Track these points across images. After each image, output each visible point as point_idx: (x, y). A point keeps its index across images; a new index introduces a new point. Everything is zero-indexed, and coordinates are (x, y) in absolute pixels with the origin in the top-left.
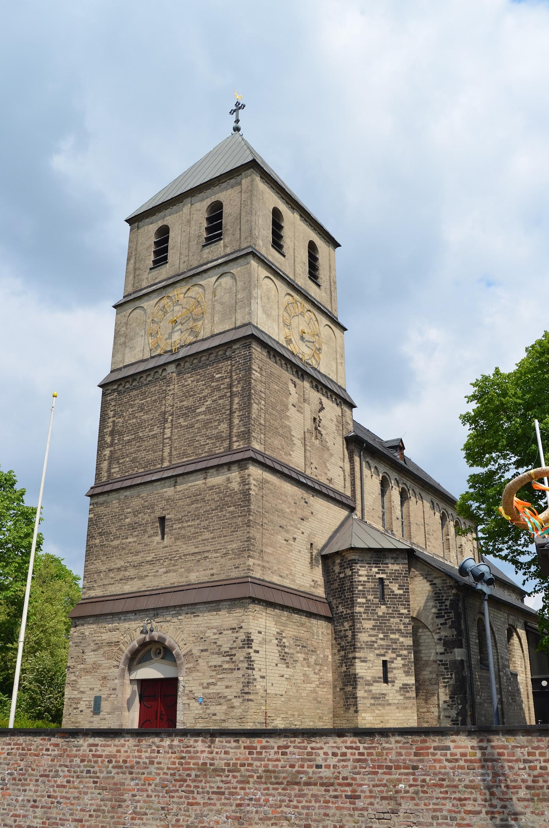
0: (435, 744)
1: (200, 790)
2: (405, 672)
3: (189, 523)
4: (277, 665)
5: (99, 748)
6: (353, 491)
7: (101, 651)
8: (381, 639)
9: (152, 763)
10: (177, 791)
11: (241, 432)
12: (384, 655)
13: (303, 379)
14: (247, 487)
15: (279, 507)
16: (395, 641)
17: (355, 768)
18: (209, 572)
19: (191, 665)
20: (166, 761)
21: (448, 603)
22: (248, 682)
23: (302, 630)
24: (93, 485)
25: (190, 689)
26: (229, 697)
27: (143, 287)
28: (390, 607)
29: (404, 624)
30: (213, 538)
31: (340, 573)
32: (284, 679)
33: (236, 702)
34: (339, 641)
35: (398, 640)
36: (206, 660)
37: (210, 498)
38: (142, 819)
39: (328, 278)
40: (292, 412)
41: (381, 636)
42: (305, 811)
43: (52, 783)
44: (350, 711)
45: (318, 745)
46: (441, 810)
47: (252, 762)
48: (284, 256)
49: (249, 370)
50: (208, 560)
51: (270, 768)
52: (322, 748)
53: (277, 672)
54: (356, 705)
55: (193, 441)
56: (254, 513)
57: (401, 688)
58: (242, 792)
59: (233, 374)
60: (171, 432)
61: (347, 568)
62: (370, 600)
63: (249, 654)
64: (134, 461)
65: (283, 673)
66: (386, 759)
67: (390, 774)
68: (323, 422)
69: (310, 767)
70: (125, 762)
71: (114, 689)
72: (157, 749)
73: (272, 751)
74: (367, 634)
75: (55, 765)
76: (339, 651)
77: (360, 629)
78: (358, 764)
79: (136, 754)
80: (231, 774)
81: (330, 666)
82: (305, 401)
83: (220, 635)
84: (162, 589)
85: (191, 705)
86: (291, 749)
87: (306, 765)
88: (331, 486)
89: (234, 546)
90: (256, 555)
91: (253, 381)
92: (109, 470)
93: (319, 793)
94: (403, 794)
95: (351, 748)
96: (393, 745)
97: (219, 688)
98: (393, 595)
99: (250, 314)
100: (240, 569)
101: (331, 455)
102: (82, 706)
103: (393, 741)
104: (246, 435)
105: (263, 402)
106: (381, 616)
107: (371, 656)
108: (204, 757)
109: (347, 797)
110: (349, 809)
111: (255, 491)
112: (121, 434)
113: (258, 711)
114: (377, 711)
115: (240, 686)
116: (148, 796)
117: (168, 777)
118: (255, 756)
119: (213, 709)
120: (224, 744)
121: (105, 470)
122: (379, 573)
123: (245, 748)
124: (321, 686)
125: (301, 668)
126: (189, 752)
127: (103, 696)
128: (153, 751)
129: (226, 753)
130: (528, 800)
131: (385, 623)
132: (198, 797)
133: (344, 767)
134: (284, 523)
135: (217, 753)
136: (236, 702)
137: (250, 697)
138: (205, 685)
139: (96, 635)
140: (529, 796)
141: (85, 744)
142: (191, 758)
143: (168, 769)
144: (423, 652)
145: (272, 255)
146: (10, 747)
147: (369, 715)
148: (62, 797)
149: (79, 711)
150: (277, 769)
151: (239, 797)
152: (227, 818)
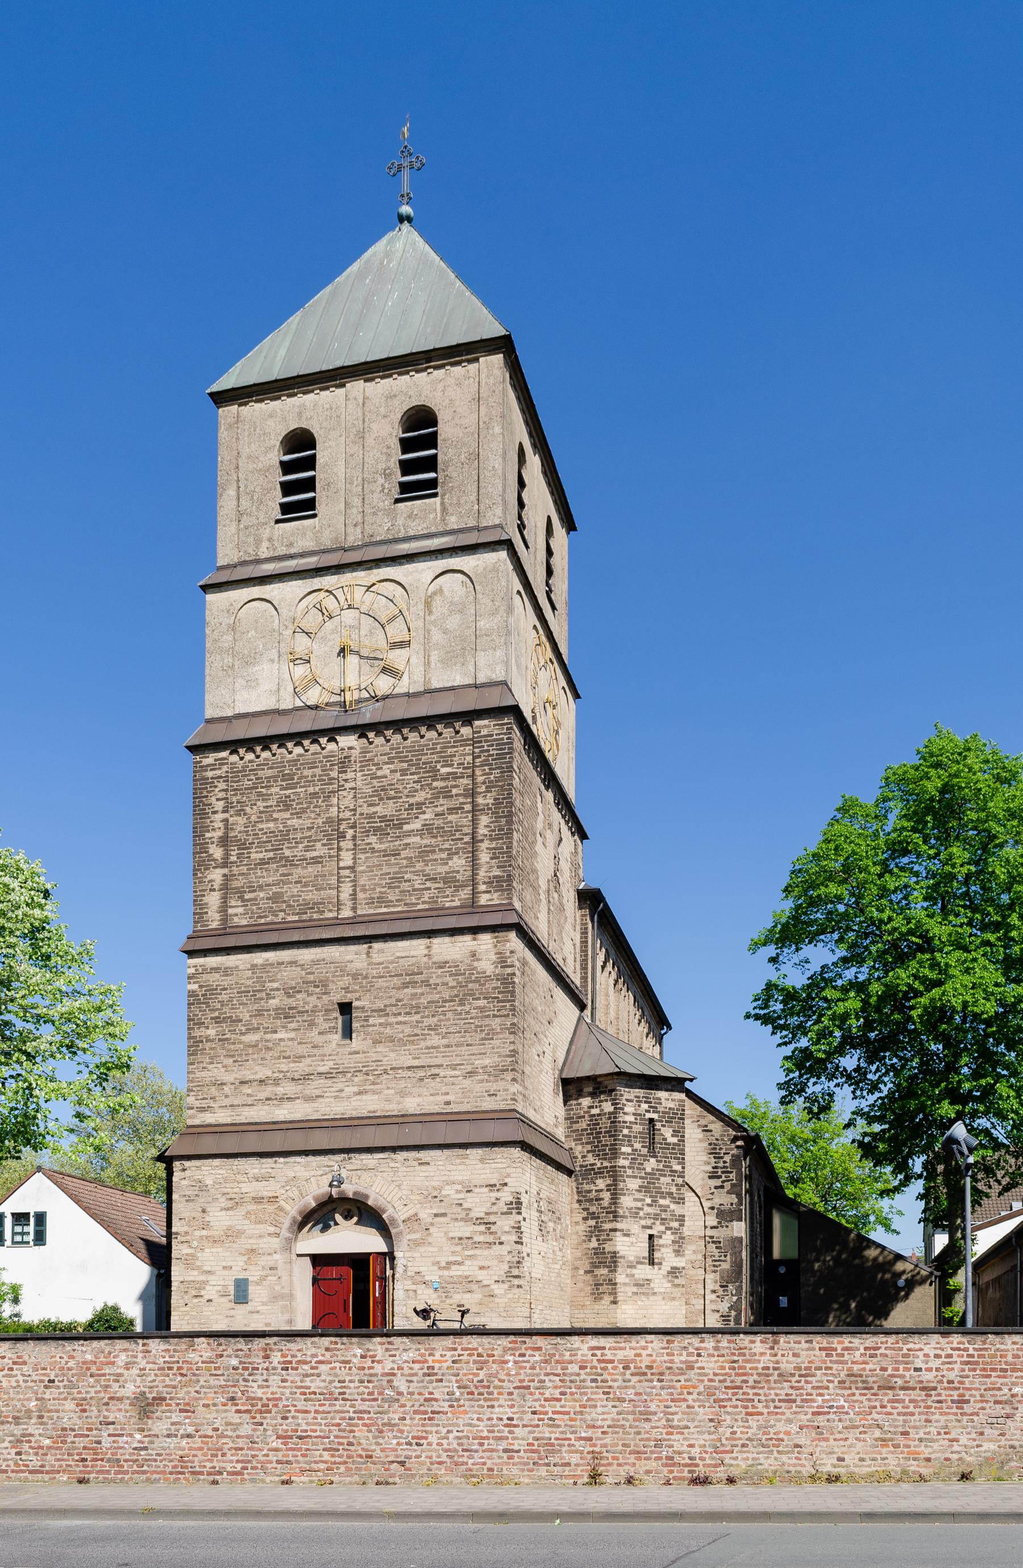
1: (763, 1398)
2: (675, 1251)
5: (606, 1352)
7: (242, 1211)
8: (648, 1205)
9: (692, 1368)
10: (731, 1399)
11: (495, 877)
12: (650, 1228)
14: (509, 970)
16: (664, 1209)
17: (963, 1370)
19: (417, 1236)
21: (727, 1158)
26: (485, 1283)
28: (661, 1161)
29: (677, 1185)
30: (448, 1046)
33: (499, 1289)
35: (669, 1207)
36: (445, 1229)
37: (438, 981)
38: (683, 1433)
41: (648, 1201)
42: (901, 1418)
44: (603, 1302)
45: (917, 1346)
50: (438, 1080)
52: (921, 1350)
54: (613, 1293)
57: (669, 1273)
58: (820, 1398)
59: (478, 772)
60: (354, 858)
62: (636, 1150)
67: (1005, 1377)
69: (906, 1369)
70: (650, 1367)
73: (858, 1353)
74: (631, 1198)
75: (538, 1375)
76: (585, 1219)
77: (622, 1189)
78: (967, 1367)
79: (666, 1358)
80: (803, 1379)
83: (469, 1194)
84: (351, 1119)
85: (419, 1292)
87: (901, 1367)
89: (487, 1062)
92: (224, 908)
93: (919, 1398)
95: (959, 1349)
96: (1010, 1346)
97: (469, 1269)
100: (498, 1098)
102: (209, 1292)
103: (1010, 1342)
104: (503, 883)
106: (649, 1174)
107: (635, 1227)
108: (766, 1360)
110: (956, 1414)
114: (639, 1303)
115: (506, 1267)
116: (688, 1407)
117: (716, 1384)
118: (835, 1358)
120: (792, 1345)
121: (215, 908)
123: (820, 1349)
127: (251, 1279)
128: (689, 1354)
129: (795, 1355)
131: (654, 1183)
135: (783, 1355)
136: (499, 1289)
138: (443, 1264)
139: (227, 1185)
141: (585, 1346)
143: (715, 1374)
146: (456, 1353)
148: (554, 1413)
149: (203, 1300)
151: (815, 1404)
152: (801, 1428)
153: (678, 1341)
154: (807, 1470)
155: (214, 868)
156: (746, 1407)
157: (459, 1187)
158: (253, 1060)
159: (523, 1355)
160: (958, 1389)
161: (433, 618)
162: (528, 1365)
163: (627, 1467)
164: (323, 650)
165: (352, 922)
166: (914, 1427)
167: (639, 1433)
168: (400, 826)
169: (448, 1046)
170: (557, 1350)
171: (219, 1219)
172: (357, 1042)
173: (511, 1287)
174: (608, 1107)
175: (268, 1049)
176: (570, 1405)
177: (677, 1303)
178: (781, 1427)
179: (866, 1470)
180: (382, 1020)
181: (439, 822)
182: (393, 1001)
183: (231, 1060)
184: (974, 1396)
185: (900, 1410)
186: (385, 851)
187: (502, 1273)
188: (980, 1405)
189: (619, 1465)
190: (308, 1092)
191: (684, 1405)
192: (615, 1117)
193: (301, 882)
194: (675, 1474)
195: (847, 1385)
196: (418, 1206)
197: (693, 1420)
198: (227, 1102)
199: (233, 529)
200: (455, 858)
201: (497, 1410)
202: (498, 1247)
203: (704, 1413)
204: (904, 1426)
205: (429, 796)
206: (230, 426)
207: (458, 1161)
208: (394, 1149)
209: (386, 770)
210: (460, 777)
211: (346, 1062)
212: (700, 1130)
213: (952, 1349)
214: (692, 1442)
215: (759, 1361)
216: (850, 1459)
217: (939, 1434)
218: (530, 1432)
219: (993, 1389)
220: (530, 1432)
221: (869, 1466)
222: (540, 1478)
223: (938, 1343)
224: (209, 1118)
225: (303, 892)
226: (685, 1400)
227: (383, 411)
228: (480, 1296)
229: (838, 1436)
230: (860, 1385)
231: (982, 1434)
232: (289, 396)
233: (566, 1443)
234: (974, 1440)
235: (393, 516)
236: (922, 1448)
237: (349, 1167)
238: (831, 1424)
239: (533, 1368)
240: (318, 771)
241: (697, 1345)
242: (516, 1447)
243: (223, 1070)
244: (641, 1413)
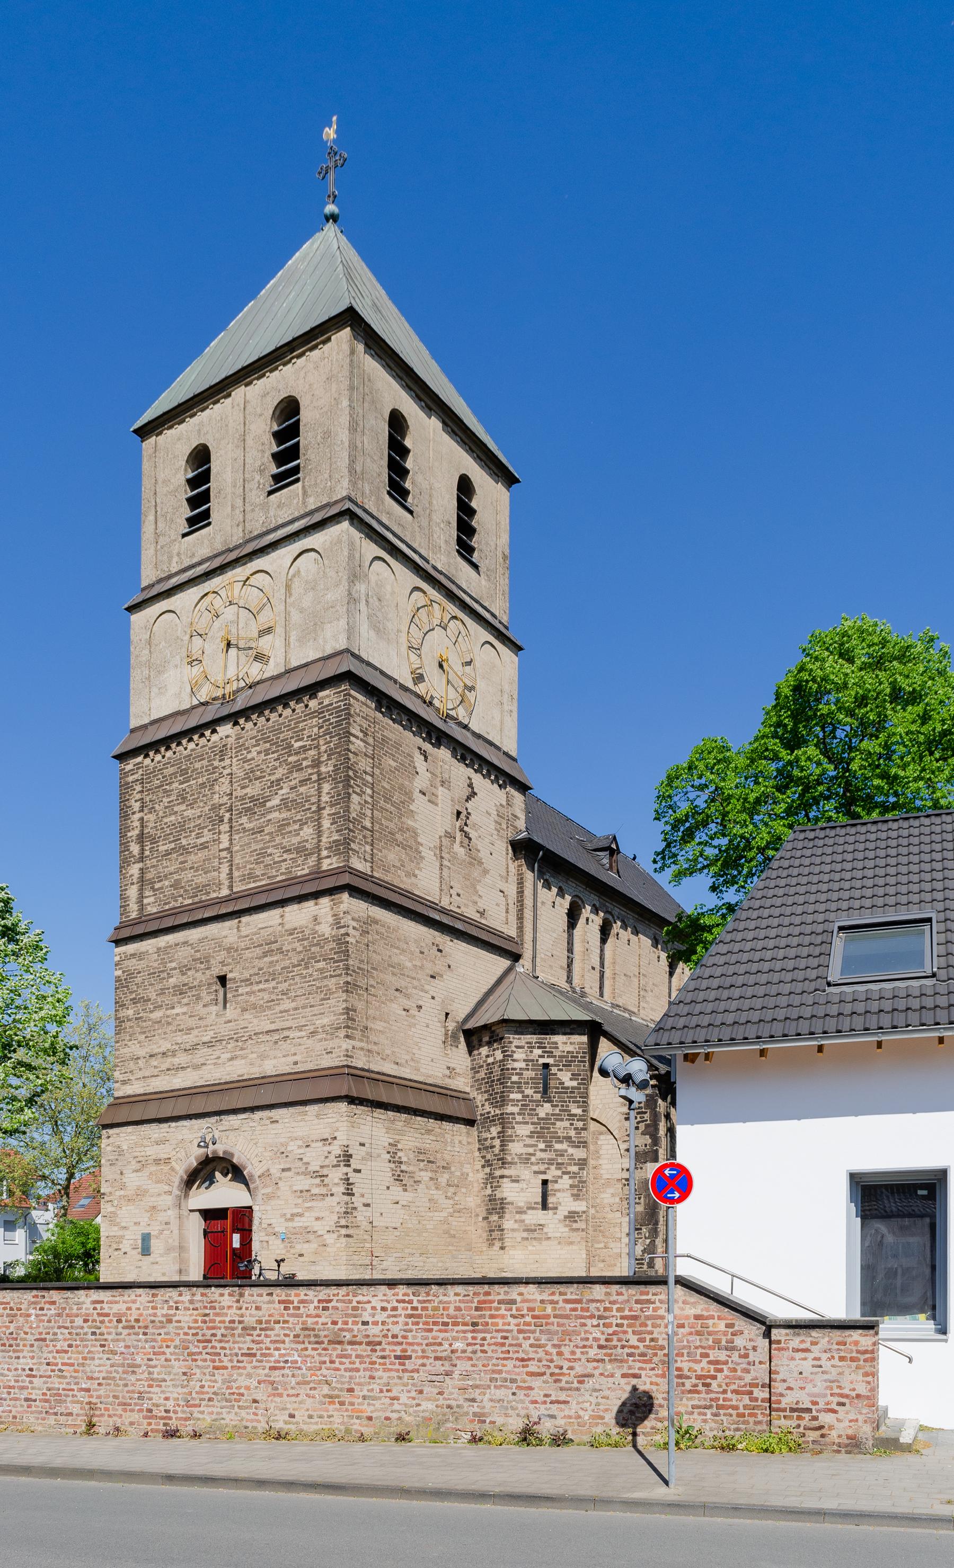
0: (500, 1297)
1: (228, 1352)
2: (573, 1195)
3: (261, 986)
5: (105, 1305)
6: (520, 928)
7: (146, 1172)
8: (541, 1150)
9: (170, 1321)
12: (545, 1173)
13: (438, 745)
14: (343, 931)
15: (395, 960)
16: (561, 1154)
17: (407, 1324)
19: (268, 1190)
23: (429, 1138)
24: (117, 924)
26: (320, 1233)
27: (174, 570)
29: (576, 1129)
30: (296, 1009)
31: (487, 1056)
32: (399, 1206)
33: (330, 1239)
34: (484, 1153)
37: (289, 948)
38: (160, 1386)
40: (420, 804)
41: (542, 1146)
42: (348, 1374)
43: (51, 1348)
45: (365, 1299)
46: (500, 1372)
48: (411, 512)
51: (309, 1325)
52: (369, 1302)
54: (501, 1239)
55: (263, 854)
57: (566, 1217)
58: (277, 1353)
60: (231, 840)
64: (176, 885)
65: (398, 1198)
67: (446, 1331)
68: (472, 818)
70: (137, 1321)
73: (312, 1306)
74: (521, 1144)
76: (483, 1166)
78: (410, 1321)
79: (151, 1311)
87: (350, 1320)
88: (483, 921)
89: (325, 1021)
90: (357, 1034)
91: (351, 756)
92: (141, 897)
94: (459, 1354)
95: (404, 1301)
97: (307, 1220)
101: (486, 872)
104: (343, 847)
105: (369, 791)
107: (526, 1173)
108: (232, 1314)
109: (396, 1357)
110: (398, 1371)
112: (154, 841)
114: (530, 1248)
116: (166, 1360)
117: (190, 1337)
118: (292, 1311)
122: (543, 1057)
123: (280, 1302)
124: (457, 1214)
128: (170, 1308)
129: (257, 1308)
130: (598, 1361)
132: (225, 1359)
134: (402, 983)
138: (288, 1216)
140: (599, 1357)
142: (217, 1315)
143: (190, 1328)
144: (604, 1167)
148: (63, 1364)
152: (259, 1383)
153: (163, 1294)
154: (262, 1426)
156: (214, 1361)
159: (42, 1309)
160: (401, 1344)
161: (292, 599)
162: (46, 1318)
163: (115, 1418)
164: (214, 646)
166: (359, 1384)
167: (126, 1385)
168: (263, 804)
169: (296, 1009)
170: (67, 1303)
171: (133, 1180)
172: (231, 1012)
173: (339, 1236)
176: (74, 1357)
177: (574, 1247)
178: (243, 1381)
179: (314, 1428)
180: (248, 989)
181: (293, 796)
182: (256, 970)
184: (416, 1352)
185: (348, 1366)
188: (420, 1361)
189: (110, 1416)
190: (195, 1061)
191: (163, 1358)
194: (153, 1426)
195: (301, 1339)
197: (170, 1373)
198: (140, 1074)
199: (152, 551)
200: (305, 827)
201: (21, 1360)
202: (329, 1198)
203: (178, 1367)
204: (350, 1383)
206: (150, 456)
208: (253, 1109)
209: (254, 754)
213: (398, 1301)
214: (168, 1395)
215: (226, 1315)
216: (300, 1416)
217: (381, 1391)
218: (45, 1383)
219: (434, 1344)
220: (45, 1383)
221: (316, 1423)
222: (50, 1426)
224: (129, 1090)
226: (164, 1353)
227: (259, 410)
228: (316, 1246)
229: (291, 1392)
230: (312, 1339)
231: (421, 1392)
232: (192, 416)
233: (71, 1393)
234: (414, 1399)
235: (265, 507)
236: (365, 1406)
237: (221, 1128)
238: (285, 1379)
239: (49, 1321)
240: (205, 762)
241: (176, 1298)
242: (33, 1397)
244: (129, 1366)
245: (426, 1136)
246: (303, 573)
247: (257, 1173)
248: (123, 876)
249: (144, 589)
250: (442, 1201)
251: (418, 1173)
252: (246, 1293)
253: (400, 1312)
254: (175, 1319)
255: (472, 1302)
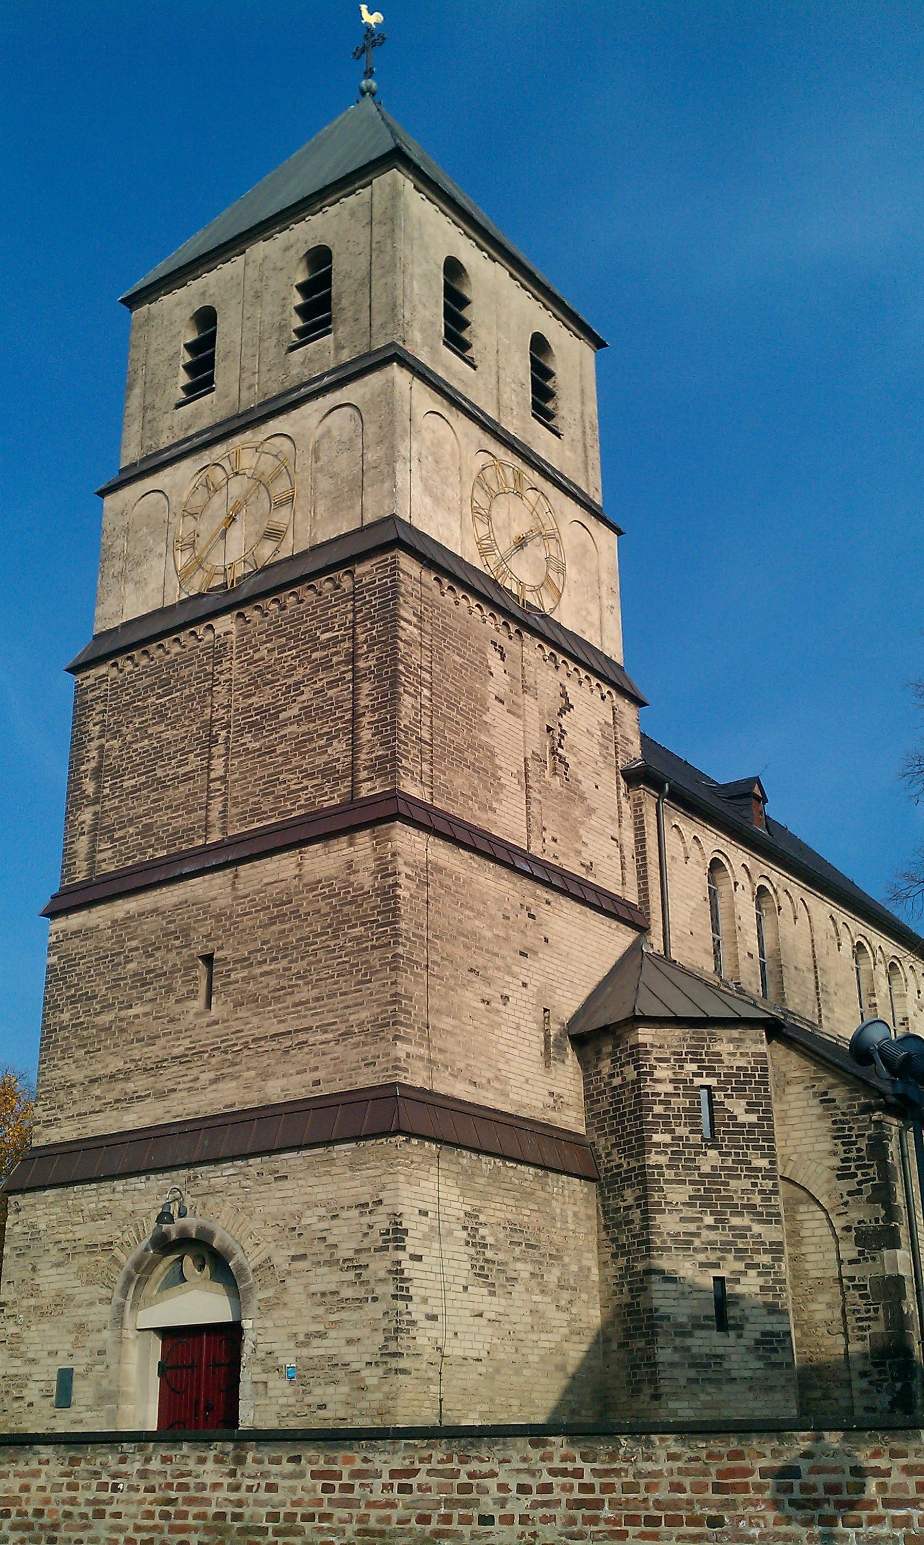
3: (266, 968)
4: (465, 1288)
6: (644, 891)
8: (709, 1227)
9: (100, 1514)
11: (377, 758)
12: (717, 1266)
14: (390, 880)
15: (468, 926)
16: (741, 1233)
18: (310, 1077)
19: (270, 1293)
20: (133, 1509)
21: (863, 1144)
22: (397, 1330)
25: (267, 1348)
26: (354, 1366)
29: (762, 1192)
30: (317, 999)
31: (612, 1076)
32: (483, 1321)
33: (371, 1377)
36: (304, 1280)
39: (578, 417)
40: (496, 713)
44: (642, 1397)
45: (485, 1467)
47: (329, 1510)
48: (475, 367)
49: (392, 620)
50: (306, 1049)
51: (373, 1524)
52: (493, 1474)
53: (466, 1304)
54: (653, 1381)
55: (273, 783)
56: (408, 939)
57: (758, 1342)
59: (358, 630)
60: (226, 766)
61: (628, 1063)
63: (399, 1263)
65: (482, 1307)
66: (645, 1500)
68: (569, 736)
69: (466, 1520)
70: (39, 1513)
71: (101, 1353)
72: (111, 1482)
73: (377, 1483)
74: (676, 1217)
76: (614, 1256)
78: (578, 1514)
79: (66, 1494)
81: (595, 1292)
82: (525, 689)
85: (270, 1385)
86: (421, 1478)
89: (364, 1015)
90: (414, 1034)
91: (401, 645)
92: (91, 856)
95: (564, 1473)
96: (664, 1466)
97: (333, 1344)
98: (734, 1125)
99: (393, 495)
100: (377, 1068)
101: (591, 811)
102: (32, 1392)
103: (662, 1454)
104: (388, 765)
105: (426, 692)
106: (707, 1175)
111: (408, 889)
112: (117, 774)
113: (423, 1396)
114: (703, 1397)
115: (380, 1338)
118: (336, 1495)
119: (319, 1393)
121: (82, 856)
122: (700, 1075)
124: (576, 1338)
125: (525, 1296)
126: (184, 1487)
128: (103, 1487)
129: (271, 1488)
133: (545, 1520)
134: (479, 961)
136: (371, 1377)
137: (403, 1363)
138: (301, 1338)
139: (61, 1229)
142: (190, 1501)
143: (138, 1529)
144: (810, 1258)
145: (447, 364)
147: (686, 1404)
150: (387, 1528)
155: (86, 806)
157: (322, 1211)
158: (106, 1047)
165: (219, 846)
168: (276, 716)
171: (51, 1280)
174: (631, 1073)
175: (122, 1031)
177: (778, 1396)
180: (245, 973)
183: (83, 1052)
186: (258, 750)
187: (376, 1350)
190: (159, 1086)
192: (639, 1088)
193: (171, 807)
196: (273, 1245)
198: (74, 1110)
200: (335, 742)
205: (308, 671)
207: (322, 1170)
210: (342, 641)
211: (202, 1037)
212: (816, 1101)
213: (553, 1472)
223: (524, 1460)
224: (54, 1135)
225: (174, 818)
240: (195, 668)
243: (73, 1066)
245: (523, 1203)
246: (335, 433)
247: (251, 1263)
248: (70, 823)
249: (122, 471)
250: (551, 1312)
251: (512, 1266)
252: (250, 1456)
253: (557, 1494)
254: (109, 1509)
255: (706, 1473)
